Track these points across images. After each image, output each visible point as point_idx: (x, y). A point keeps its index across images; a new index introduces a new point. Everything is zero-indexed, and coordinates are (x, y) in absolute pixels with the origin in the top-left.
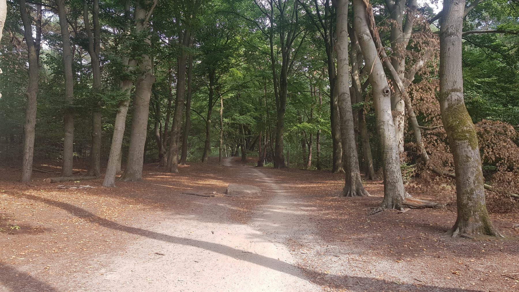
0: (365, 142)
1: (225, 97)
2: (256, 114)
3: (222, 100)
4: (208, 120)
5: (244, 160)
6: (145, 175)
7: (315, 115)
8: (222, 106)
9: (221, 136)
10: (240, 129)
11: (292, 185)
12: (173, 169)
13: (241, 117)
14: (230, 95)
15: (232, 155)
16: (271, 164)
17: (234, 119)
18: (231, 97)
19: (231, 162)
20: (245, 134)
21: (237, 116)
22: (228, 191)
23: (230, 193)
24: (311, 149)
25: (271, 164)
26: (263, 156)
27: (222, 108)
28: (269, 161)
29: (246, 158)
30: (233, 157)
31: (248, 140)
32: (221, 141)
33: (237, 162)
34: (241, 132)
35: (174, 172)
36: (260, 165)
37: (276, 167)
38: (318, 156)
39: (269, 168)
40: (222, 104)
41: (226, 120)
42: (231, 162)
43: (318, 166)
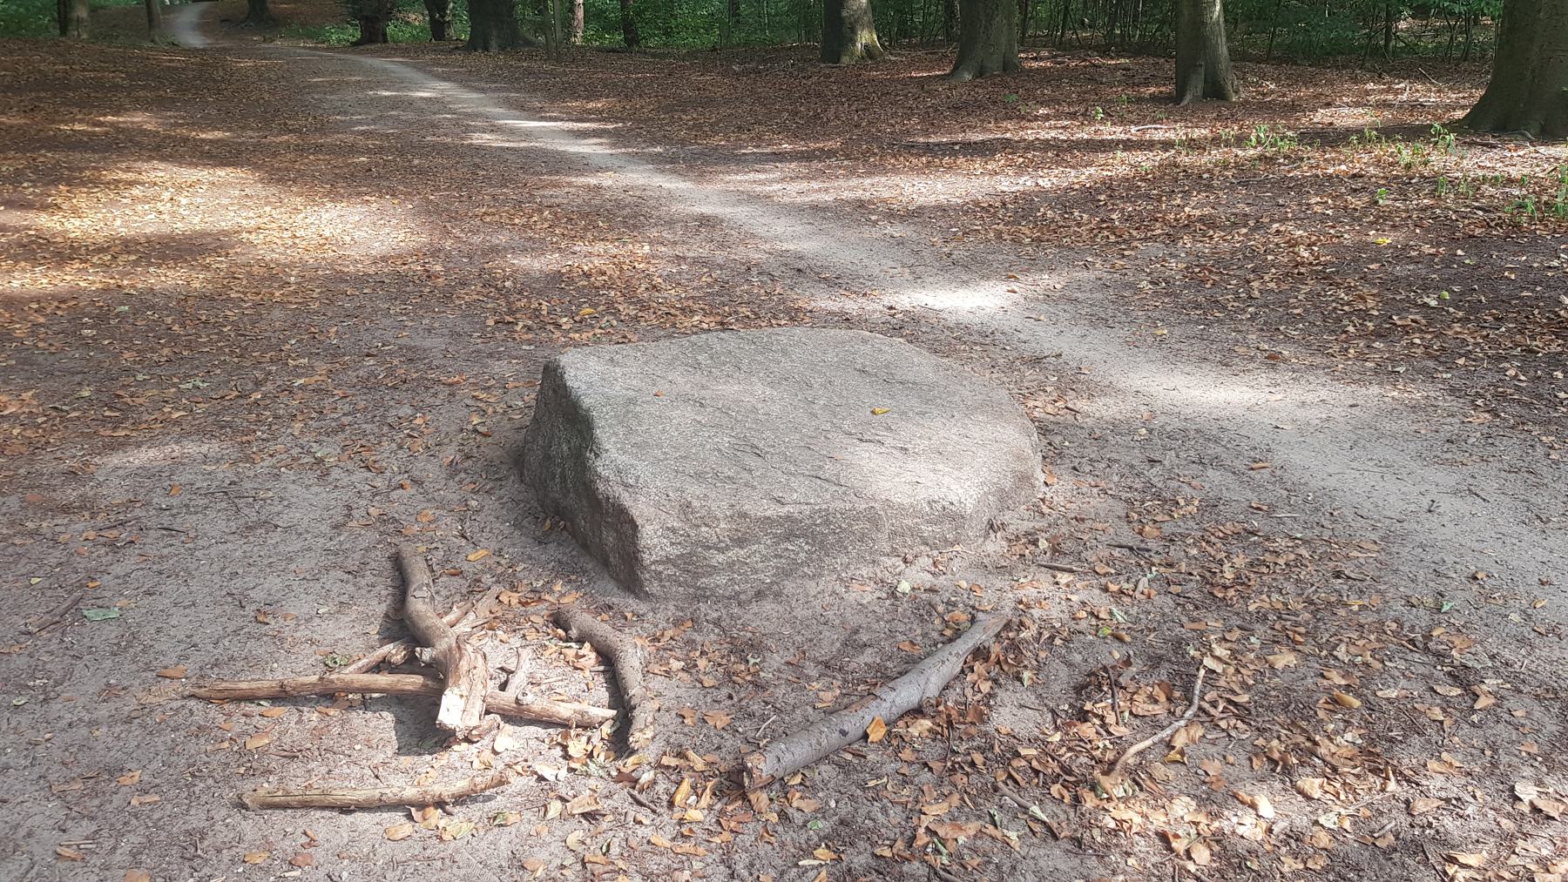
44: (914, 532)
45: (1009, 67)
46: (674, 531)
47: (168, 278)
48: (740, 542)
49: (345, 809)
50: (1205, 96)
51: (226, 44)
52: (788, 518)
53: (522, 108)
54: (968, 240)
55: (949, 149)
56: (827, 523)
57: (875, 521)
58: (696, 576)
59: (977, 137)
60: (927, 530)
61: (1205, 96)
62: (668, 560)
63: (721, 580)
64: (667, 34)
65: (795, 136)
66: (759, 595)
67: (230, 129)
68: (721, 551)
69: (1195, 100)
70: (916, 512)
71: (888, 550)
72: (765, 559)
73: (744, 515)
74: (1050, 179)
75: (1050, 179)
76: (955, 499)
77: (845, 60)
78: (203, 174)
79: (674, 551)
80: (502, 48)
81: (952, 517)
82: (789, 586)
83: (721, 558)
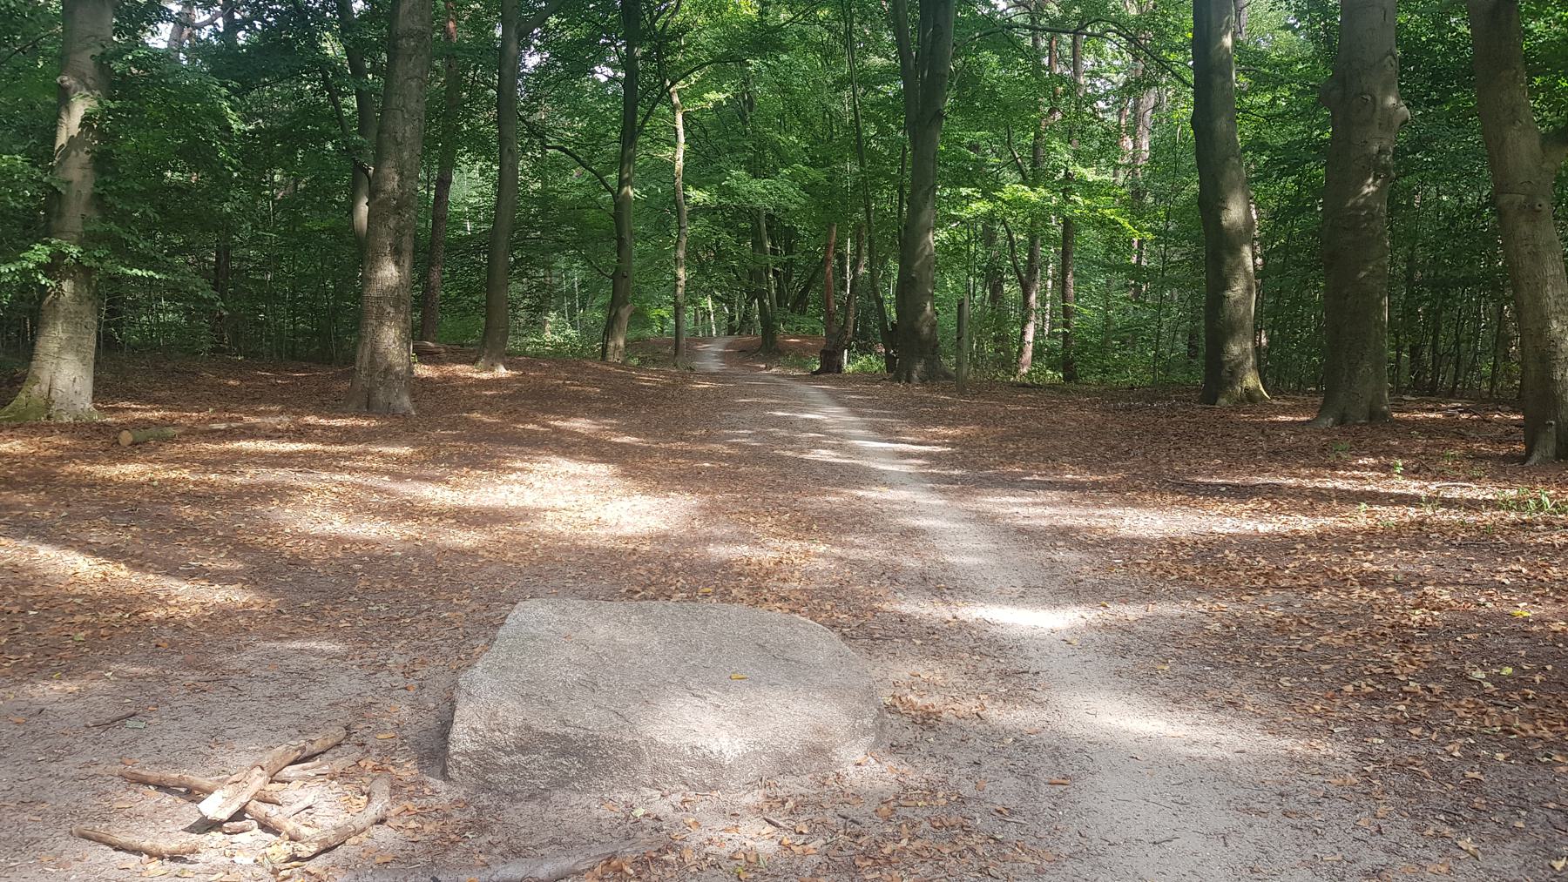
0: (1533, 212)
1: (694, 105)
2: (814, 174)
3: (679, 117)
4: (621, 186)
5: (770, 349)
6: (104, 440)
7: (1061, 153)
8: (682, 139)
9: (681, 254)
10: (755, 234)
11: (1073, 515)
12: (381, 396)
13: (757, 185)
14: (713, 96)
15: (731, 331)
16: (873, 362)
17: (728, 192)
18: (718, 104)
19: (723, 356)
20: (774, 252)
21: (736, 175)
22: (462, 738)
23: (484, 762)
24: (1033, 297)
25: (873, 362)
26: (844, 328)
27: (682, 146)
28: (865, 350)
29: (779, 338)
30: (730, 339)
31: (783, 278)
32: (681, 273)
33: (745, 354)
34: (757, 244)
35: (388, 411)
36: (831, 365)
37: (897, 370)
38: (1066, 325)
39: (865, 377)
40: (681, 131)
41: (697, 196)
42: (723, 356)
43: (1066, 366)
44: (676, 771)
45: (1376, 417)
46: (475, 730)
47: (466, 539)
48: (523, 749)
49: (119, 848)
50: (1558, 457)
51: (737, 370)
52: (565, 737)
53: (881, 431)
54: (1056, 568)
55: (1212, 491)
56: (596, 748)
57: (637, 754)
58: (486, 771)
59: (1456, 494)
60: (687, 772)
61: (1558, 457)
62: (466, 754)
63: (504, 778)
64: (1105, 371)
65: (1088, 465)
66: (532, 797)
67: (638, 436)
68: (508, 754)
69: (1545, 461)
70: (676, 752)
71: (650, 782)
72: (542, 768)
73: (529, 728)
74: (1305, 524)
75: (1305, 524)
76: (715, 749)
77: (1223, 401)
78: (572, 466)
79: (471, 747)
80: (923, 381)
81: (713, 764)
82: (558, 795)
83: (506, 759)
